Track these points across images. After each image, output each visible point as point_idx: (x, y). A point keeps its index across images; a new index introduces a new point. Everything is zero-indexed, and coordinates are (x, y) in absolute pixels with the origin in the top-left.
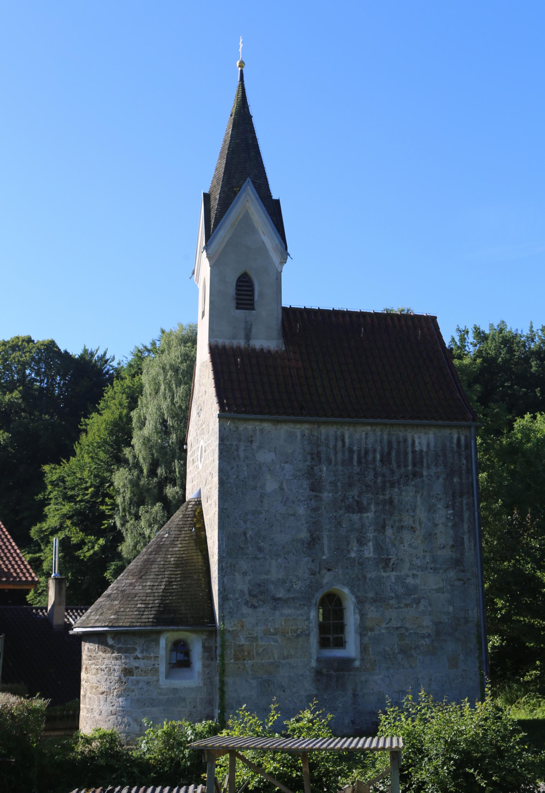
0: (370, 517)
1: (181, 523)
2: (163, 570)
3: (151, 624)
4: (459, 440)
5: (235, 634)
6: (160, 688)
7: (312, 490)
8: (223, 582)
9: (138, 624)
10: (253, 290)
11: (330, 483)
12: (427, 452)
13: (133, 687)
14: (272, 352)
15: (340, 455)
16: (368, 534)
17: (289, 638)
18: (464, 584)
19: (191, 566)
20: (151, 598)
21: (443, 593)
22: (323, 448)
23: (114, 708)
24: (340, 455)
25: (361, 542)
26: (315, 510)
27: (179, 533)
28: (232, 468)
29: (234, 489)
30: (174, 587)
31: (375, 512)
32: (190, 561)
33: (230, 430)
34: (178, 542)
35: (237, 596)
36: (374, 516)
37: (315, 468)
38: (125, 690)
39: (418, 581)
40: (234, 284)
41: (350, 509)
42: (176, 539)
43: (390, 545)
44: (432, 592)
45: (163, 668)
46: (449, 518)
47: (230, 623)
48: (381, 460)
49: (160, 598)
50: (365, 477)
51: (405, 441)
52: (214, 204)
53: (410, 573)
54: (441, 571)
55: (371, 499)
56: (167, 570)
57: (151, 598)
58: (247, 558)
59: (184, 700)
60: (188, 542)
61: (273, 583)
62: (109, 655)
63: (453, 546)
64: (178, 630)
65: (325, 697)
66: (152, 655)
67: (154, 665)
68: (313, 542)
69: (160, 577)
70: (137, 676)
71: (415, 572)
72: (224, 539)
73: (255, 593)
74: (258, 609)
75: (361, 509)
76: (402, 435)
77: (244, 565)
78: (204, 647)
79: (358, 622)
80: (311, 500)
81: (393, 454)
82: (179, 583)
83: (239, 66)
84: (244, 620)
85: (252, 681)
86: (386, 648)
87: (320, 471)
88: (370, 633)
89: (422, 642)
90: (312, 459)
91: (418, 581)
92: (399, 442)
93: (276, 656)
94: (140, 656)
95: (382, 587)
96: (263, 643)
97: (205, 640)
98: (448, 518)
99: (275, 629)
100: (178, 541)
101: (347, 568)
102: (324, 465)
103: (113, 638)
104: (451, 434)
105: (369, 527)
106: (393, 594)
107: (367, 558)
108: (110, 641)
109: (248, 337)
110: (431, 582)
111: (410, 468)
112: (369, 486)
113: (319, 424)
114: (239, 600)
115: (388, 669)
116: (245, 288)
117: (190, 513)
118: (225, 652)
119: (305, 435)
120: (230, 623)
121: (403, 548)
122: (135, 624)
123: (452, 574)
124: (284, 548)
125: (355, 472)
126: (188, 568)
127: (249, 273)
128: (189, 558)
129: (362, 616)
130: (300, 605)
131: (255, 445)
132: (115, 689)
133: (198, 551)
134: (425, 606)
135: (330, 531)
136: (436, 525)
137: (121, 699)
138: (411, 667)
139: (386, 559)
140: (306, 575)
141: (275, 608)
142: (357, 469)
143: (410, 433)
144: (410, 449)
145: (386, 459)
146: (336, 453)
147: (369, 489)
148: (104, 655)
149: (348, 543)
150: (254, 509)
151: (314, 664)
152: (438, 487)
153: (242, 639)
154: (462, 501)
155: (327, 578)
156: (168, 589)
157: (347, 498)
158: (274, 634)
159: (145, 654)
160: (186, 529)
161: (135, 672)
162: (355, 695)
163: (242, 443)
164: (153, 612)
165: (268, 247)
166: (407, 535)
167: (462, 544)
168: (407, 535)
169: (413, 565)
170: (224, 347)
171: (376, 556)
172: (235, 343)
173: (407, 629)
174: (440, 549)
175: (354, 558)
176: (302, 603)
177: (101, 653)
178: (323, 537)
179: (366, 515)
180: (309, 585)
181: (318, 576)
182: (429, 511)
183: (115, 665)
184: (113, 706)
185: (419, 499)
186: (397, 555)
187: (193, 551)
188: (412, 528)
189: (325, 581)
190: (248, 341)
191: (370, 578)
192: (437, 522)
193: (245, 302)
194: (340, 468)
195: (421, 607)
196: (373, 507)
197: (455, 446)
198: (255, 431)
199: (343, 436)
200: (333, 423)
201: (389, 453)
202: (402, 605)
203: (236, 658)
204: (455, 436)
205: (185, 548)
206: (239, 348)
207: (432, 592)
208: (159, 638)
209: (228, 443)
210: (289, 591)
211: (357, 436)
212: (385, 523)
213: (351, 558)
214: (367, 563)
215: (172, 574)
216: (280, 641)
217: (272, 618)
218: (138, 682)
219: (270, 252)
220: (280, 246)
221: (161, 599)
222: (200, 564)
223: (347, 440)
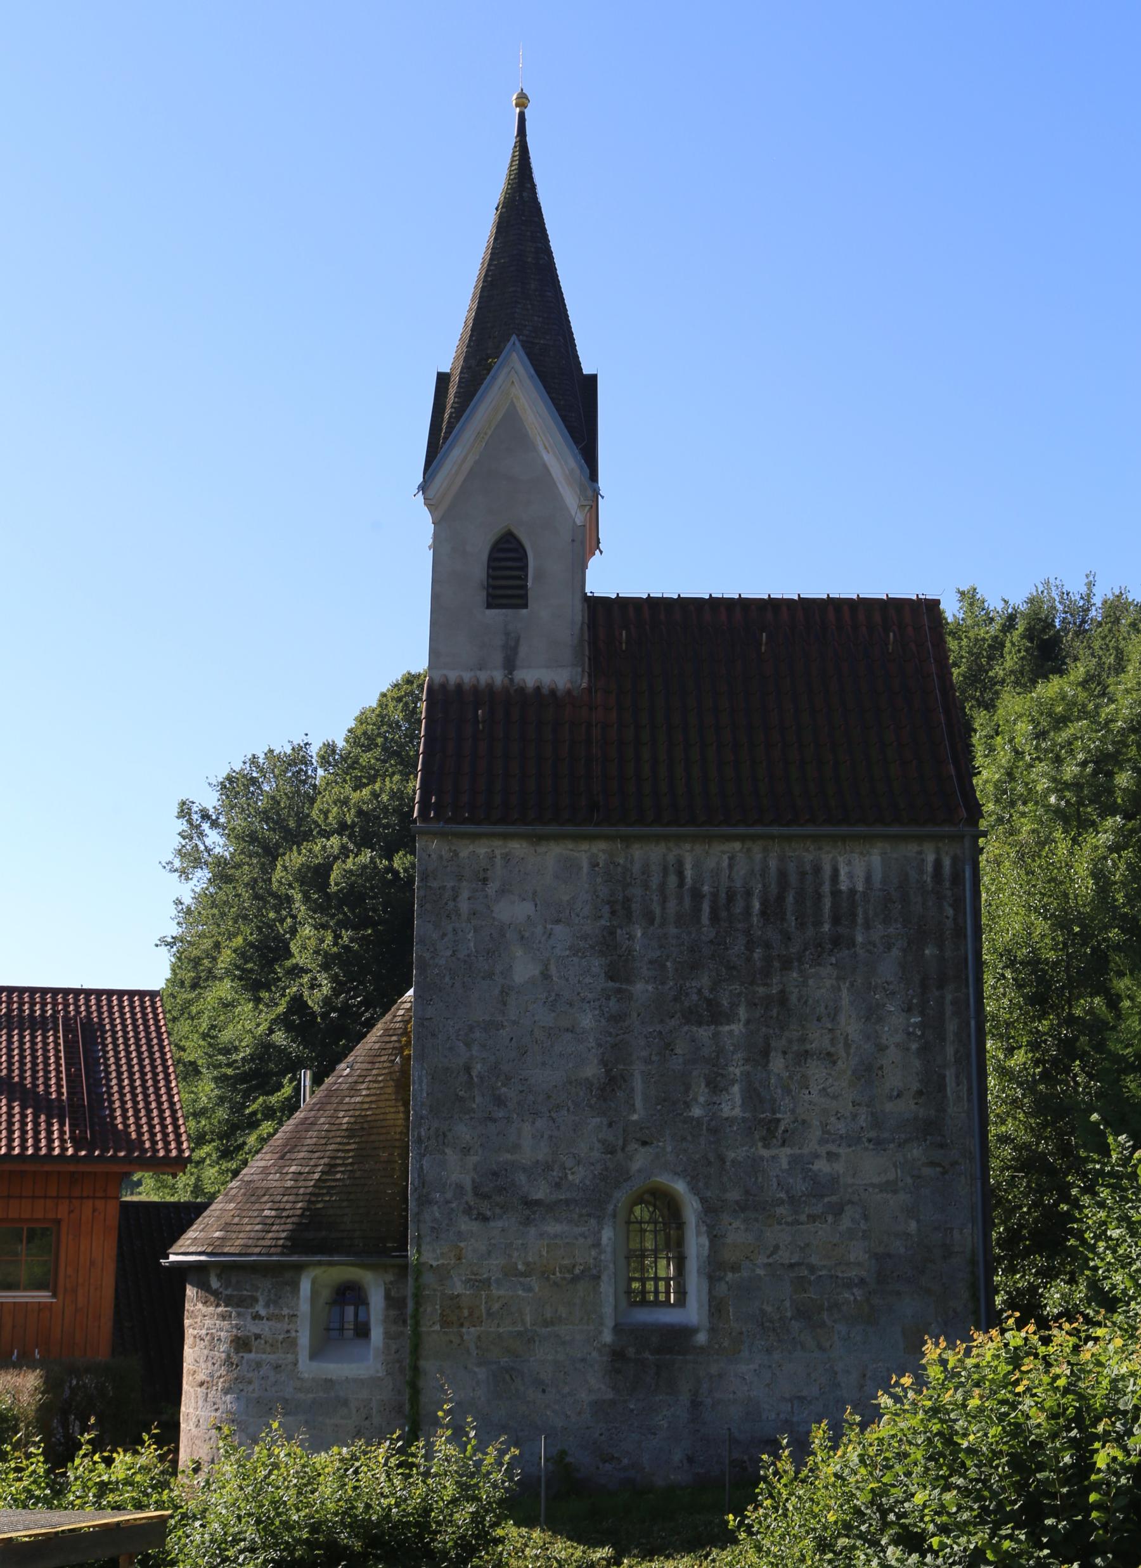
0: (737, 1033)
1: (377, 1046)
2: (323, 1141)
3: (279, 1250)
4: (938, 864)
5: (443, 1274)
6: (298, 1379)
7: (612, 979)
8: (421, 1167)
9: (257, 1250)
10: (524, 568)
11: (651, 962)
12: (864, 894)
13: (250, 1375)
14: (559, 694)
15: (672, 905)
16: (731, 1069)
17: (555, 1283)
18: (944, 1173)
19: (379, 1134)
20: (291, 1198)
21: (895, 1192)
22: (637, 891)
23: (218, 1414)
24: (672, 905)
25: (716, 1085)
26: (617, 1018)
27: (369, 1066)
28: (444, 935)
29: (447, 979)
30: (338, 1176)
31: (748, 1022)
32: (379, 1124)
33: (441, 857)
34: (364, 1086)
35: (449, 1195)
36: (744, 1031)
37: (619, 931)
38: (236, 1379)
39: (839, 1167)
40: (485, 557)
41: (691, 1016)
42: (361, 1080)
43: (779, 1091)
44: (870, 1190)
45: (304, 1339)
46: (913, 1033)
47: (434, 1250)
48: (763, 913)
49: (307, 1198)
50: (727, 949)
51: (817, 870)
52: (452, 390)
53: (822, 1151)
54: (892, 1146)
55: (740, 994)
56: (331, 1141)
57: (291, 1198)
58: (472, 1118)
59: (345, 1403)
60: (382, 1085)
61: (524, 1170)
62: (211, 1309)
63: (920, 1093)
64: (331, 1264)
65: (632, 1407)
66: (285, 1311)
67: (288, 1331)
68: (613, 1083)
69: (317, 1155)
70: (257, 1352)
71: (833, 1148)
72: (425, 1081)
73: (486, 1189)
74: (492, 1224)
75: (716, 1015)
76: (811, 858)
77: (464, 1132)
78: (387, 1296)
79: (706, 1252)
80: (608, 998)
81: (790, 899)
82: (349, 1168)
83: (517, 105)
84: (462, 1245)
85: (476, 1370)
86: (765, 1307)
87: (629, 939)
88: (730, 1276)
89: (846, 1295)
90: (613, 913)
91: (839, 1167)
92: (803, 874)
93: (528, 1319)
94: (263, 1313)
95: (760, 1179)
96: (502, 1292)
97: (391, 1283)
98: (909, 1034)
99: (527, 1264)
100: (363, 1082)
101: (684, 1139)
102: (637, 926)
103: (219, 1277)
104: (920, 853)
105: (733, 1053)
106: (783, 1195)
107: (727, 1119)
108: (215, 1284)
109: (510, 665)
110: (872, 1168)
111: (826, 927)
112: (734, 968)
113: (627, 840)
114: (454, 1205)
115: (769, 1351)
116: (510, 564)
117: (398, 1025)
118: (421, 1310)
119: (598, 865)
120: (434, 1250)
121: (807, 1097)
122: (250, 1251)
123: (916, 1152)
124: (549, 1097)
125: (703, 937)
126: (373, 1138)
127: (516, 532)
128: (377, 1117)
129: (715, 1239)
130: (581, 1216)
131: (492, 888)
132: (220, 1377)
133: (400, 1104)
134: (853, 1220)
135: (648, 1061)
136: (882, 1049)
137: (229, 1396)
138: (821, 1348)
139: (770, 1121)
140: (596, 1155)
141: (527, 1222)
142: (708, 932)
143: (828, 852)
144: (826, 888)
145: (772, 910)
146: (664, 900)
147: (735, 973)
148: (204, 1309)
149: (687, 1088)
150: (487, 1018)
151: (607, 1337)
152: (888, 969)
153: (458, 1284)
154: (943, 997)
155: (640, 1159)
156: (326, 1181)
157: (687, 994)
158: (522, 1274)
159: (271, 1310)
160: (382, 1059)
161: (254, 1344)
162: (695, 1404)
163: (465, 883)
164: (290, 1227)
165: (554, 475)
166: (816, 1071)
167: (942, 1087)
168: (816, 1071)
169: (828, 1132)
170: (459, 687)
171: (747, 1115)
172: (483, 677)
173: (812, 1269)
174: (890, 1098)
175: (699, 1120)
176: (584, 1211)
177: (200, 1306)
178: (632, 1075)
179: (727, 1028)
180: (601, 1174)
181: (620, 1155)
182: (868, 1019)
183: (221, 1330)
184: (216, 1410)
185: (845, 993)
186: (793, 1111)
187: (388, 1103)
188: (829, 1054)
189: (635, 1166)
190: (511, 674)
191: (733, 1161)
192: (884, 1041)
193: (509, 592)
194: (673, 930)
195: (846, 1223)
196: (742, 1012)
197: (929, 879)
198: (491, 858)
199: (680, 863)
200: (658, 838)
201: (781, 898)
202: (803, 1218)
203: (445, 1323)
204: (931, 858)
205: (373, 1098)
206: (490, 687)
207: (870, 1190)
208: (299, 1278)
209: (435, 884)
210: (558, 1185)
211: (711, 863)
212: (769, 1045)
213: (692, 1118)
214: (728, 1130)
215: (338, 1151)
216: (537, 1289)
217: (520, 1242)
218: (259, 1365)
219: (560, 487)
220: (578, 472)
221: (309, 1201)
222: (399, 1130)
223: (689, 873)
